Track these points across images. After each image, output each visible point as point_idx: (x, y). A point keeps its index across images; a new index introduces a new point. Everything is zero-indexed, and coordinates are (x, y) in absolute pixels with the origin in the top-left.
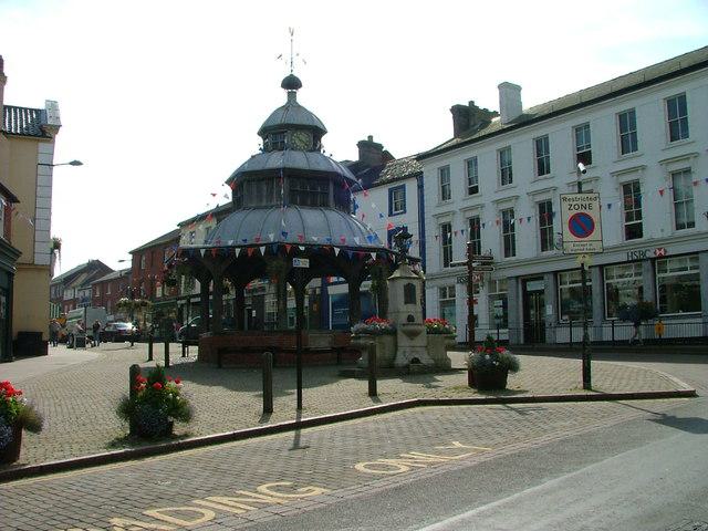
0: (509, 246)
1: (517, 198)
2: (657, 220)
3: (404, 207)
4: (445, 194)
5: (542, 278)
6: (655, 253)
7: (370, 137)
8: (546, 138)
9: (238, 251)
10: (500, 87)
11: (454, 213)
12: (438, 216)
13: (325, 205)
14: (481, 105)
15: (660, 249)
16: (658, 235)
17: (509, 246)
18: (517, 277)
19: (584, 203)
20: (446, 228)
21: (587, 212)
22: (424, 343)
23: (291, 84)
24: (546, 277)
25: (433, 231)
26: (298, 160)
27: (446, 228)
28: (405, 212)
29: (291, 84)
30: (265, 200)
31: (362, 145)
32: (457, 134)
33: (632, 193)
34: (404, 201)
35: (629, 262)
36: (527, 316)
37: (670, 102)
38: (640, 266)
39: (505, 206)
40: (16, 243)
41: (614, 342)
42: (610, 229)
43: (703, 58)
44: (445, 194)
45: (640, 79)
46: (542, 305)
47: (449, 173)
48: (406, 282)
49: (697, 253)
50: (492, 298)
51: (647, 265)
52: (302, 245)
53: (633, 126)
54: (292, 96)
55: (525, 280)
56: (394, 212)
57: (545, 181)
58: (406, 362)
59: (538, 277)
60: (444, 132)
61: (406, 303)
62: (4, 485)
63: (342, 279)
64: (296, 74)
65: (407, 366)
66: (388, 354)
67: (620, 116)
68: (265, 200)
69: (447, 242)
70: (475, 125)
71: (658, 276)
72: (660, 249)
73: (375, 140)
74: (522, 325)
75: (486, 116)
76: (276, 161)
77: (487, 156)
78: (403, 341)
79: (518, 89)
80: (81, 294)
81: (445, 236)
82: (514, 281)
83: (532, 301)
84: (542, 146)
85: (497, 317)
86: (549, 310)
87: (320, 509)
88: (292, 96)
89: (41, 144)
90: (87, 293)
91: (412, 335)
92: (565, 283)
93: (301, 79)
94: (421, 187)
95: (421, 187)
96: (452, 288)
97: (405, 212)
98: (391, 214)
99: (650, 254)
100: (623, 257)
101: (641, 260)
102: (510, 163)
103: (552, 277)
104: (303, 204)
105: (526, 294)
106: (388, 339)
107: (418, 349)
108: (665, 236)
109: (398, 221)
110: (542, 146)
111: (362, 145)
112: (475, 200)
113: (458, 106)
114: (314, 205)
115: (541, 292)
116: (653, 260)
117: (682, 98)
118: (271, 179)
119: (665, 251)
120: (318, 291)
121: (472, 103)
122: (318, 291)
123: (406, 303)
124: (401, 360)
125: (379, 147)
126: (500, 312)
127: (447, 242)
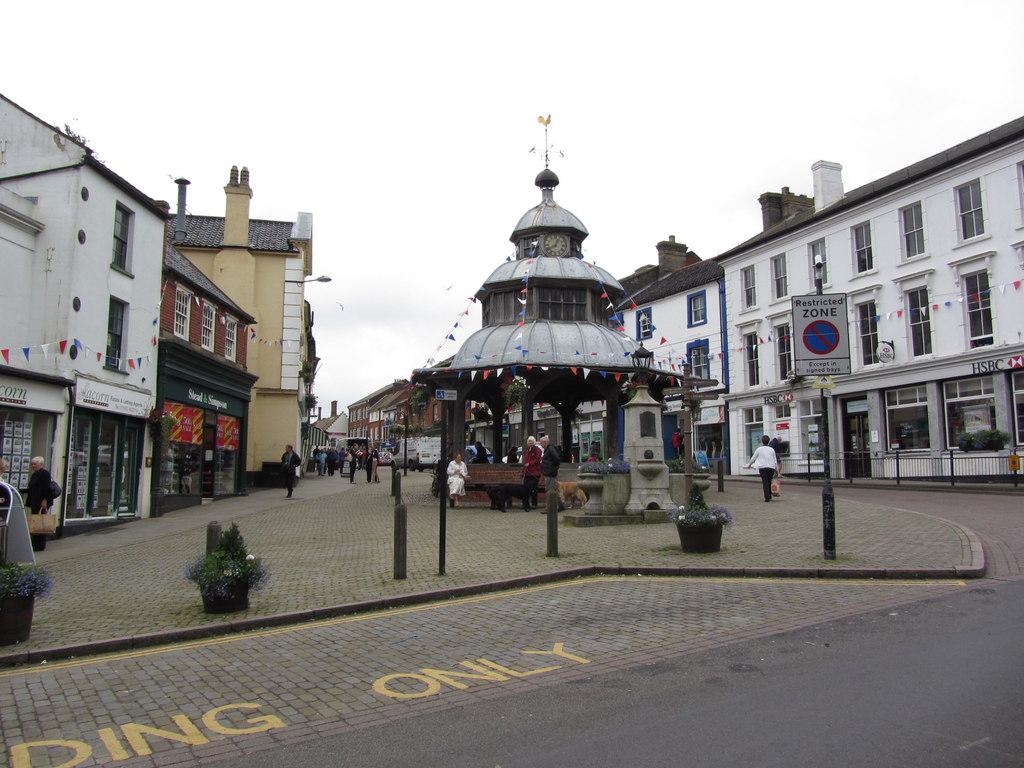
2: (950, 336)
3: (704, 317)
4: (750, 298)
5: (865, 398)
6: (1010, 363)
7: (672, 237)
9: (474, 373)
10: (815, 168)
11: (760, 322)
12: (742, 326)
13: (581, 319)
14: (796, 191)
15: (1017, 358)
19: (824, 308)
20: (752, 339)
21: (829, 319)
22: (666, 484)
23: (547, 181)
24: (869, 396)
25: (736, 342)
26: (552, 267)
27: (752, 339)
28: (705, 322)
29: (547, 181)
31: (663, 247)
33: (918, 300)
34: (705, 309)
35: (974, 376)
38: (991, 381)
40: (252, 368)
41: (953, 479)
42: (950, 336)
43: (1020, 127)
44: (750, 298)
46: (864, 432)
48: (645, 409)
49: (924, 383)
50: (804, 422)
51: (1000, 379)
52: (545, 365)
53: (978, 202)
54: (548, 201)
56: (694, 323)
58: (641, 508)
59: (861, 396)
60: (753, 224)
61: (642, 436)
62: (8, 673)
64: (552, 168)
65: (642, 513)
66: (619, 498)
69: (752, 355)
70: (789, 215)
71: (1016, 392)
72: (1017, 358)
73: (678, 241)
74: (842, 456)
75: (805, 202)
76: (525, 270)
77: (796, 253)
78: (638, 482)
79: (837, 168)
80: (387, 416)
81: (750, 349)
83: (854, 426)
85: (812, 445)
86: (875, 436)
87: (760, 639)
88: (548, 201)
89: (288, 260)
90: (392, 415)
91: (651, 475)
92: (955, 396)
93: (557, 174)
94: (722, 292)
95: (722, 292)
96: (759, 411)
97: (705, 322)
98: (690, 325)
99: (1004, 365)
100: (967, 370)
101: (990, 373)
104: (556, 318)
105: (847, 418)
106: (620, 480)
107: (658, 492)
109: (699, 333)
111: (663, 247)
113: (769, 194)
114: (568, 319)
115: (865, 415)
116: (1008, 373)
121: (786, 189)
123: (642, 436)
124: (636, 504)
125: (683, 248)
126: (815, 438)
127: (752, 355)
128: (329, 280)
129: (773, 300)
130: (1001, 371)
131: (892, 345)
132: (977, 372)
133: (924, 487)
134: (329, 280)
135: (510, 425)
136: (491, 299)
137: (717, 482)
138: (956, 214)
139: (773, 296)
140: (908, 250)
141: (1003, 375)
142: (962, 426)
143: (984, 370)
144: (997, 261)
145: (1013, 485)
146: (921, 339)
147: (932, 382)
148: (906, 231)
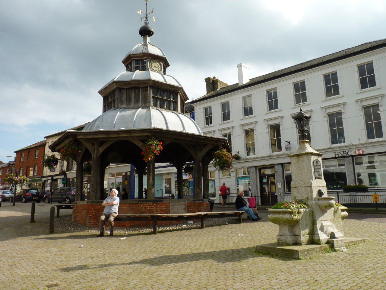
0: (250, 150)
1: (233, 128)
6: (355, 152)
8: (228, 103)
15: (359, 150)
16: (356, 142)
17: (250, 150)
18: (256, 167)
24: (276, 167)
30: (133, 103)
32: (208, 93)
35: (335, 158)
36: (262, 190)
37: (361, 68)
39: (246, 128)
45: (343, 54)
47: (211, 111)
55: (260, 168)
57: (275, 113)
59: (272, 167)
63: (168, 164)
67: (295, 85)
68: (133, 103)
72: (359, 150)
74: (259, 195)
77: (216, 105)
82: (254, 169)
84: (225, 107)
99: (352, 153)
102: (211, 114)
103: (280, 167)
105: (262, 176)
108: (361, 142)
110: (225, 107)
112: (249, 119)
115: (273, 175)
117: (303, 83)
118: (138, 88)
119: (363, 151)
120: (128, 174)
122: (128, 174)
128: (7, 157)
129: (243, 117)
130: (350, 156)
131: (289, 142)
132: (337, 156)
133: (370, 211)
134: (7, 157)
135: (67, 179)
136: (122, 109)
137: (228, 202)
138: (204, 117)
139: (222, 121)
140: (206, 123)
141: (351, 158)
142: (44, 188)
143: (341, 155)
144: (258, 125)
145: (375, 209)
146: (277, 144)
147: (253, 167)
148: (223, 112)
